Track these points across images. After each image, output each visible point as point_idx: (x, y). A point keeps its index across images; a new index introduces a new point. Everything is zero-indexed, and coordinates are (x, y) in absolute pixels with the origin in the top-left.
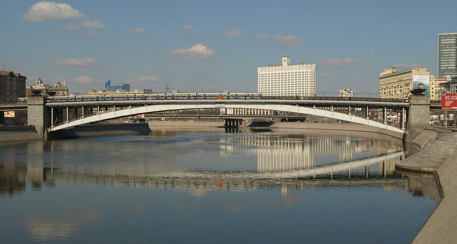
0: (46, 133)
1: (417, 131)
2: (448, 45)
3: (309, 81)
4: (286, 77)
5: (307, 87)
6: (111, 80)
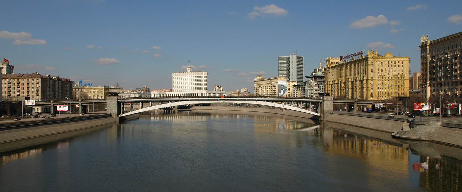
0: (118, 118)
1: (327, 114)
5: (202, 85)
6: (82, 80)
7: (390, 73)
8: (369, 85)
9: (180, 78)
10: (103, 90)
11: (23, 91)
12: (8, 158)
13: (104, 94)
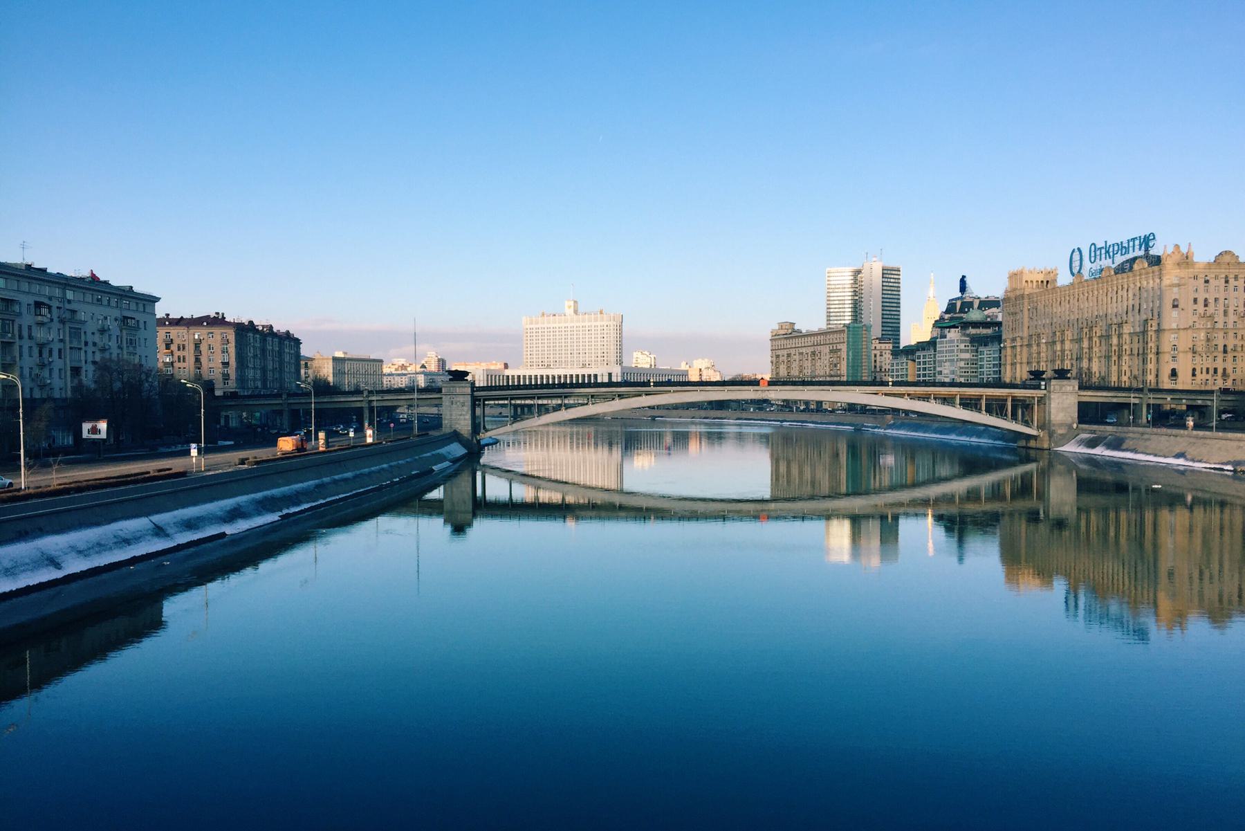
7: (1231, 311)
8: (1166, 348)
9: (552, 330)
10: (328, 364)
11: (181, 353)
12: (1168, 608)
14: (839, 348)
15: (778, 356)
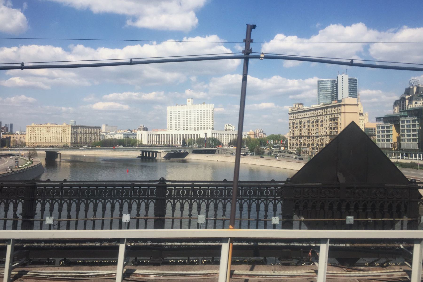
2: (325, 89)
3: (209, 120)
4: (190, 114)
13: (70, 134)
14: (336, 116)
15: (293, 124)
